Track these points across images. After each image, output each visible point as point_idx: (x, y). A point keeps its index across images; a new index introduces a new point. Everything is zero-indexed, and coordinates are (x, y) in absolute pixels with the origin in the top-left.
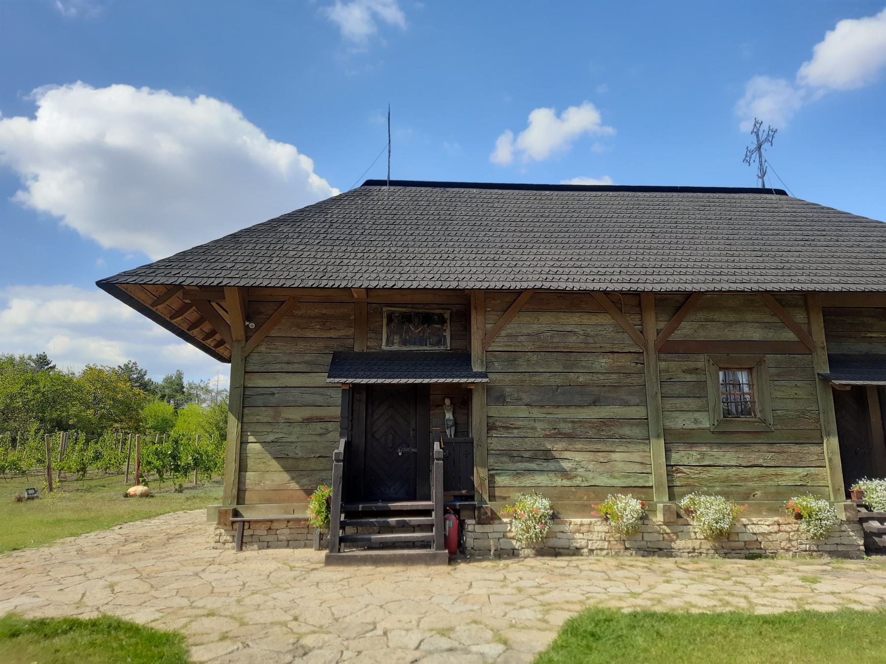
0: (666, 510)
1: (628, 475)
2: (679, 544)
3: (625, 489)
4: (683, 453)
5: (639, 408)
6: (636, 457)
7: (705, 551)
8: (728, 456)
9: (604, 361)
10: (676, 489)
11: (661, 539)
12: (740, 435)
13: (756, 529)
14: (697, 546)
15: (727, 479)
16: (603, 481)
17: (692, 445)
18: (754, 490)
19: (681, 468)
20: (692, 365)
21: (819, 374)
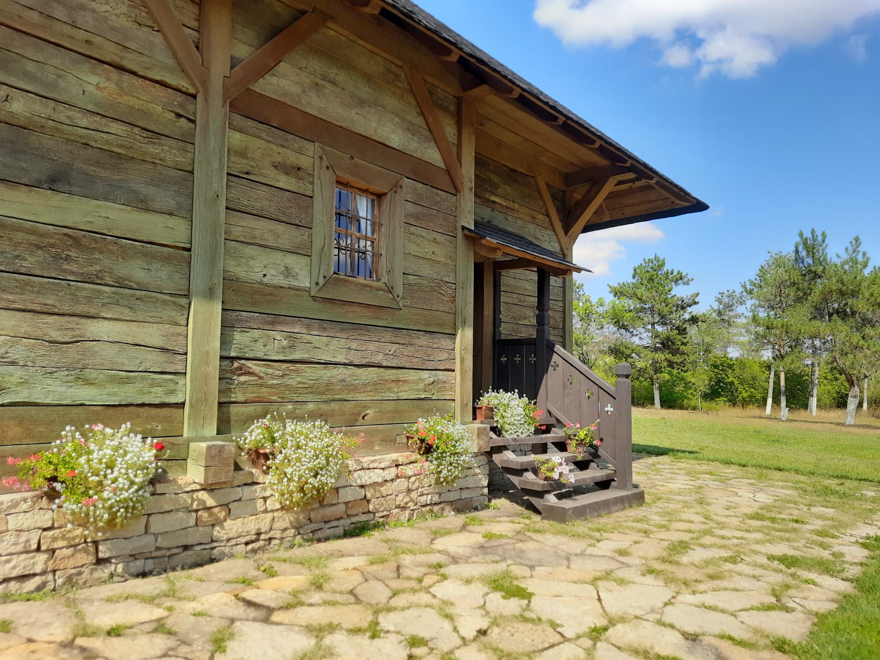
0: (213, 457)
1: (125, 377)
2: (232, 527)
3: (113, 413)
4: (256, 334)
5: (172, 222)
6: (153, 334)
7: (278, 534)
8: (335, 348)
9: (94, 79)
10: (234, 409)
11: (192, 522)
12: (357, 309)
13: (367, 478)
14: (264, 527)
15: (328, 387)
16: (53, 390)
17: (275, 320)
18: (365, 407)
19: (249, 364)
20: (292, 158)
21: (463, 228)
